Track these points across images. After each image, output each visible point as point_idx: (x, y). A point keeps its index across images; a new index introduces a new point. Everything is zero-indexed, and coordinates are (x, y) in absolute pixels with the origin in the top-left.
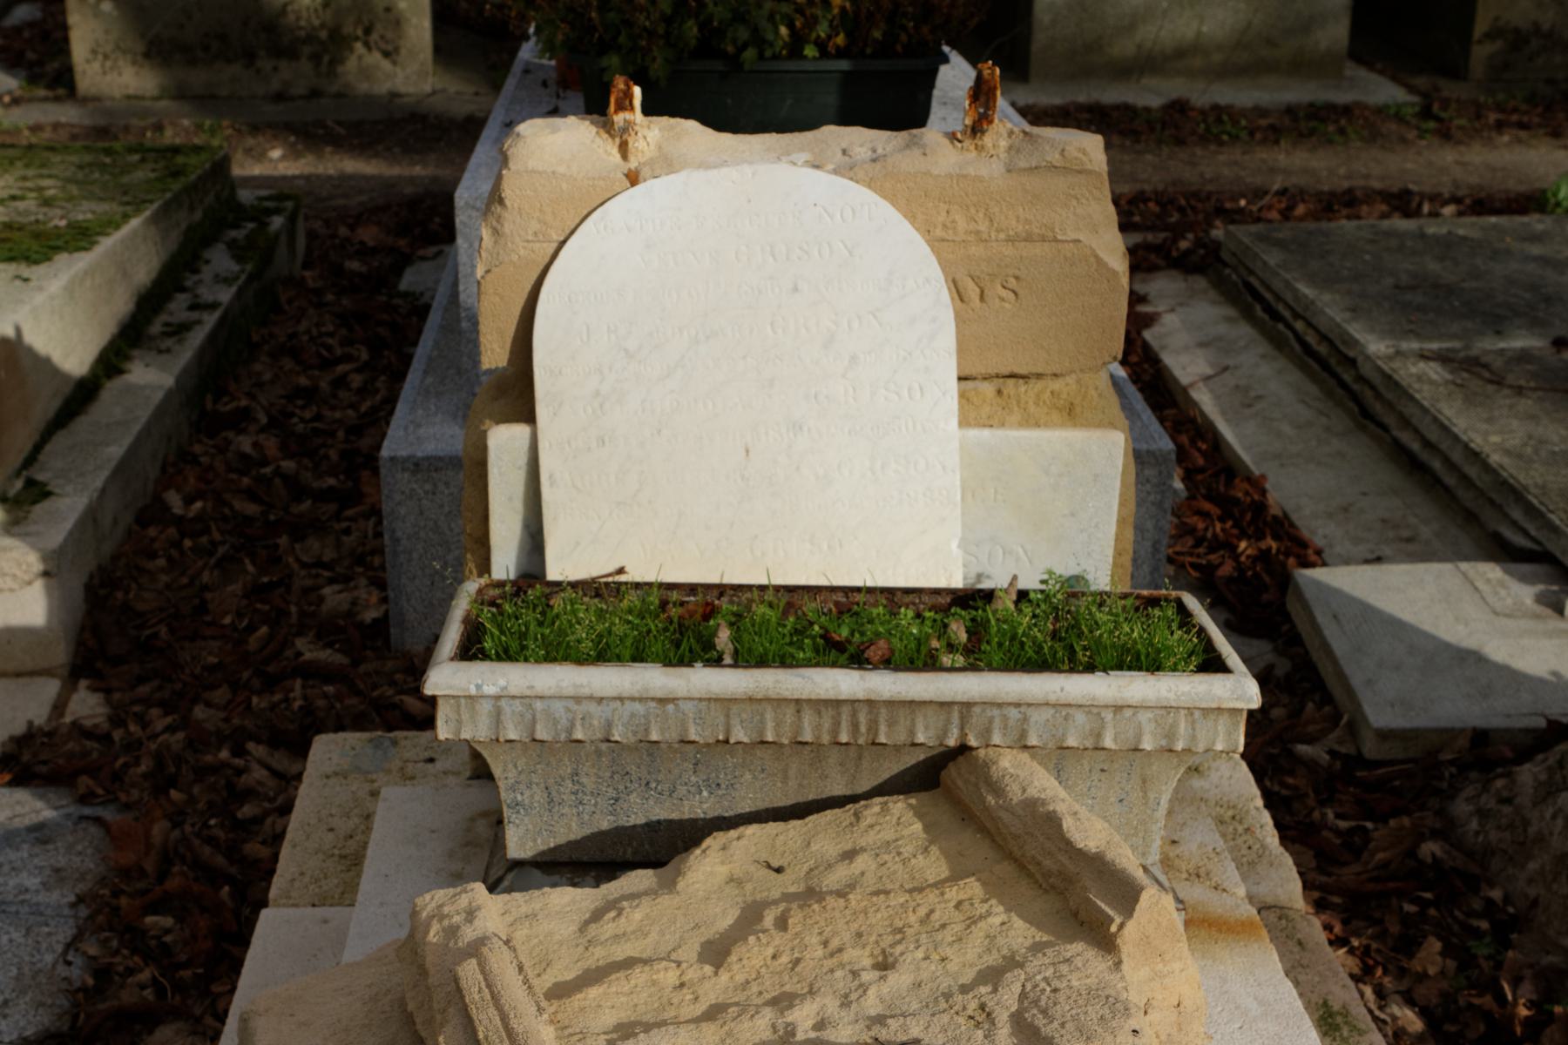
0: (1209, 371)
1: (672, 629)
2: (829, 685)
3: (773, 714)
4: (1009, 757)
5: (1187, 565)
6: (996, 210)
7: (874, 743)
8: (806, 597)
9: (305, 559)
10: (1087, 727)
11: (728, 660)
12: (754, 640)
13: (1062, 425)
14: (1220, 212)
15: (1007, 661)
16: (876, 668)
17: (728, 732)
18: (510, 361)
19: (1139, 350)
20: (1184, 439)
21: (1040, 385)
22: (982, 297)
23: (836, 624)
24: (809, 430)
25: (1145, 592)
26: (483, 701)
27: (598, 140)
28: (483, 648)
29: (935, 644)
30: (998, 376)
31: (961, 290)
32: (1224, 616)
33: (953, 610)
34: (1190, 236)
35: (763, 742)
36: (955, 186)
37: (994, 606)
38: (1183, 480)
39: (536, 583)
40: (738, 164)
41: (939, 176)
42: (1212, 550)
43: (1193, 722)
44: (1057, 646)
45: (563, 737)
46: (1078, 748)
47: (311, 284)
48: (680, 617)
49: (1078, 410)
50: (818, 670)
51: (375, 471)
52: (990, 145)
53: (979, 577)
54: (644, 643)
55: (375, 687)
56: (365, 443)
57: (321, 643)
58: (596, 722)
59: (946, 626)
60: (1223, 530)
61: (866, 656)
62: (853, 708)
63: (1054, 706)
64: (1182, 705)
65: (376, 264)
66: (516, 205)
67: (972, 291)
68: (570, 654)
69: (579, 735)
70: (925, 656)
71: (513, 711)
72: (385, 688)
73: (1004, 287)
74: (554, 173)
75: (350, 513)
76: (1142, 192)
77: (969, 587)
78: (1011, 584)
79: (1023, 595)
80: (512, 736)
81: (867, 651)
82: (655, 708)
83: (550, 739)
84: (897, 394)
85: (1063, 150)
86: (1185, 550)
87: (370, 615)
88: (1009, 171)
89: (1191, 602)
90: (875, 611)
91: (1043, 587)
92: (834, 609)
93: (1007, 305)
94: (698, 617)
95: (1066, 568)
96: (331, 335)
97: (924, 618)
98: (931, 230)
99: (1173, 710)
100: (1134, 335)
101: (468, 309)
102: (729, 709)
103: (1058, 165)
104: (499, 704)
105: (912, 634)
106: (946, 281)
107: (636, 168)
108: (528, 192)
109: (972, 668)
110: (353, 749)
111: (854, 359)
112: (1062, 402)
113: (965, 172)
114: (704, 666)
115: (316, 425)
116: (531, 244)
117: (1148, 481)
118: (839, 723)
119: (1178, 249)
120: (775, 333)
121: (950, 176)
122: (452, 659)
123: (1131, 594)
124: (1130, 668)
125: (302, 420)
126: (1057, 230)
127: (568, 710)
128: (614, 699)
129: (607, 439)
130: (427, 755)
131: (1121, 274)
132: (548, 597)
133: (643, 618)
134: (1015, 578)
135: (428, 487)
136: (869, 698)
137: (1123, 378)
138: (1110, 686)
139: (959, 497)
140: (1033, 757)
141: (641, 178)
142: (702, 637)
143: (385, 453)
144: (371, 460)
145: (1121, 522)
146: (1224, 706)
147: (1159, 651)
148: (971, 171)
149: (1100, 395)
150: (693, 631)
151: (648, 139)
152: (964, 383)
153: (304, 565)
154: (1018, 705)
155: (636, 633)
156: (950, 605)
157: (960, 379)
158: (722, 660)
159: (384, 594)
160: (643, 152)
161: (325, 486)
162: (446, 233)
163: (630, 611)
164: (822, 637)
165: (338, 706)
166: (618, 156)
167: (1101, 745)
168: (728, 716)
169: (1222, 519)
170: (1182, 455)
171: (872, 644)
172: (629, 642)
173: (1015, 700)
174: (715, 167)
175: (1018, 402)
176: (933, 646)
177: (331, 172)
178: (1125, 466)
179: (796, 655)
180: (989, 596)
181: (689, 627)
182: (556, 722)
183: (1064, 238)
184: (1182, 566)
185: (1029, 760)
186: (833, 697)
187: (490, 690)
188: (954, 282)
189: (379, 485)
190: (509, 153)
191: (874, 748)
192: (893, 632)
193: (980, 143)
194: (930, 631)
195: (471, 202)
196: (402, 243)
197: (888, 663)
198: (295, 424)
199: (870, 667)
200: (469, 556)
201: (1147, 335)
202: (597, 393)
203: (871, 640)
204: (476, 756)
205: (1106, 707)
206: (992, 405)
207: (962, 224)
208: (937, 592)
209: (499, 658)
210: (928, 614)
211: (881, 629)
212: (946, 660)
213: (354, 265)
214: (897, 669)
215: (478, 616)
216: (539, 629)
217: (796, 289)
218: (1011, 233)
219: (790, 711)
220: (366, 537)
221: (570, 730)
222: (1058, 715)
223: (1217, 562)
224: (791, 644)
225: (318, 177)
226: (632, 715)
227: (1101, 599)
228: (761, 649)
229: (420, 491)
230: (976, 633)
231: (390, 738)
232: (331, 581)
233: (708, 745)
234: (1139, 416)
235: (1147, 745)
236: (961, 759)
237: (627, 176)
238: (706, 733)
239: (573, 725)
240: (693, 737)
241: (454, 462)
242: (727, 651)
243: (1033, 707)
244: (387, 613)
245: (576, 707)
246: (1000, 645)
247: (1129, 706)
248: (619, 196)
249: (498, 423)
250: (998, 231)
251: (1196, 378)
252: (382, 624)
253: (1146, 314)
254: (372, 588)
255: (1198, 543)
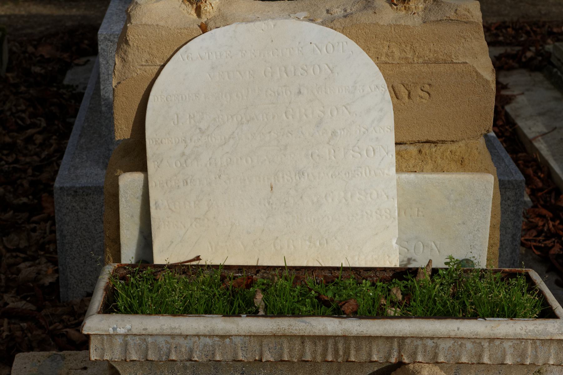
0: (545, 130)
1: (228, 294)
2: (320, 327)
3: (288, 344)
4: (427, 369)
5: (533, 248)
6: (417, 45)
7: (347, 361)
8: (307, 274)
9: (9, 246)
10: (473, 351)
11: (261, 313)
12: (276, 300)
13: (457, 171)
14: (551, 34)
15: (426, 311)
16: (348, 317)
17: (261, 355)
18: (132, 135)
19: (503, 118)
20: (530, 171)
21: (444, 146)
22: (409, 97)
23: (324, 290)
24: (308, 175)
25: (507, 269)
26: (117, 337)
27: (183, 5)
28: (117, 305)
29: (383, 301)
30: (419, 142)
31: (397, 92)
32: (554, 277)
33: (394, 281)
34: (533, 49)
35: (282, 361)
36: (393, 31)
37: (418, 278)
38: (530, 196)
39: (148, 266)
40: (265, 20)
41: (384, 25)
42: (547, 238)
43: (536, 348)
44: (456, 303)
45: (164, 358)
46: (468, 363)
47: (12, 81)
48: (232, 286)
49: (466, 161)
50: (314, 318)
51: (51, 194)
52: (413, 7)
53: (409, 260)
54: (212, 302)
55: (51, 324)
56: (44, 176)
57: (19, 297)
58: (183, 350)
59: (389, 290)
60: (554, 226)
61: (343, 309)
62: (335, 340)
63: (453, 338)
64: (529, 337)
65: (50, 69)
66: (135, 44)
67: (404, 93)
68: (168, 308)
69: (173, 357)
70: (378, 309)
71: (135, 343)
72: (57, 324)
73: (422, 90)
74: (157, 25)
75: (35, 218)
76: (504, 22)
77: (403, 266)
78: (428, 265)
79: (435, 271)
80: (134, 358)
81: (343, 307)
82: (218, 341)
83: (156, 359)
84: (360, 153)
85: (456, 10)
86: (531, 238)
87: (48, 281)
88: (424, 22)
89: (535, 275)
90: (347, 282)
91: (447, 266)
92: (323, 281)
93: (424, 101)
94: (243, 286)
95: (460, 255)
96: (23, 111)
97: (377, 286)
98: (379, 57)
99: (524, 341)
100: (500, 108)
101: (106, 99)
102: (262, 342)
103: (454, 19)
104: (126, 339)
105: (370, 295)
106: (388, 87)
107: (205, 22)
108: (143, 37)
109: (405, 316)
110: (39, 362)
111: (334, 133)
112: (457, 157)
113: (398, 23)
114: (247, 316)
115: (15, 165)
116: (144, 68)
117: (509, 199)
118: (327, 350)
119: (525, 57)
120: (288, 118)
121: (390, 25)
122: (99, 313)
123: (499, 271)
124: (498, 316)
125: (7, 163)
126: (453, 57)
127: (167, 342)
128: (195, 335)
129: (189, 181)
130: (83, 365)
131: (491, 82)
132: (154, 274)
133: (211, 287)
134: (430, 261)
135: (82, 205)
136: (344, 334)
137: (493, 137)
138: (486, 327)
139: (396, 214)
140: (441, 369)
141: (209, 28)
142: (245, 298)
143: (57, 185)
144: (48, 188)
145: (492, 227)
146: (554, 338)
147: (515, 305)
148: (402, 22)
149: (479, 153)
150: (241, 295)
151: (213, 5)
152: (399, 146)
153: (8, 250)
154: (432, 338)
155: (207, 296)
156: (392, 278)
157: (396, 144)
158: (258, 312)
159: (56, 268)
160: (209, 12)
161: (21, 202)
162: (94, 50)
163: (203, 283)
164: (316, 298)
165: (29, 335)
166: (195, 15)
167: (481, 361)
168: (261, 345)
169: (553, 220)
170: (529, 181)
171: (346, 302)
172: (203, 301)
173: (430, 335)
174: (252, 21)
175: (431, 157)
176: (382, 303)
177: (23, 13)
178: (494, 194)
179: (301, 309)
180: (415, 272)
181: (238, 292)
182: (160, 349)
183: (457, 61)
184: (530, 248)
185: (439, 371)
186: (323, 334)
187: (121, 331)
188: (393, 87)
189: (53, 202)
190: (131, 14)
191: (348, 364)
192: (359, 295)
193: (407, 6)
194: (380, 294)
195: (108, 37)
196: (66, 55)
197: (356, 314)
198: (3, 165)
199: (345, 316)
200: (108, 249)
201: (508, 108)
202: (183, 154)
203: (346, 299)
204: (112, 367)
205: (485, 339)
206: (415, 159)
207: (397, 54)
208: (385, 269)
209: (126, 312)
210: (379, 284)
211: (351, 293)
212: (391, 311)
213: (37, 69)
214: (361, 318)
215: (114, 286)
216: (150, 295)
217: (300, 92)
218: (426, 58)
219: (298, 342)
220: (45, 233)
221: (168, 354)
222: (456, 344)
223: (550, 245)
224: (298, 301)
225: (15, 16)
226: (205, 345)
227: (482, 273)
228: (281, 305)
229: (78, 207)
230: (407, 295)
231: (60, 355)
232: (25, 260)
233: (249, 362)
234: (503, 160)
235: (509, 361)
236: (399, 370)
237: (200, 27)
238: (249, 356)
239: (170, 352)
240: (241, 358)
241: (99, 190)
242: (261, 307)
243: (441, 339)
244: (58, 278)
245: (172, 341)
246: (422, 301)
247: (498, 338)
248: (196, 39)
249: (125, 172)
250: (418, 57)
251: (537, 134)
252: (55, 286)
253: (507, 96)
254: (49, 264)
255: (539, 234)
